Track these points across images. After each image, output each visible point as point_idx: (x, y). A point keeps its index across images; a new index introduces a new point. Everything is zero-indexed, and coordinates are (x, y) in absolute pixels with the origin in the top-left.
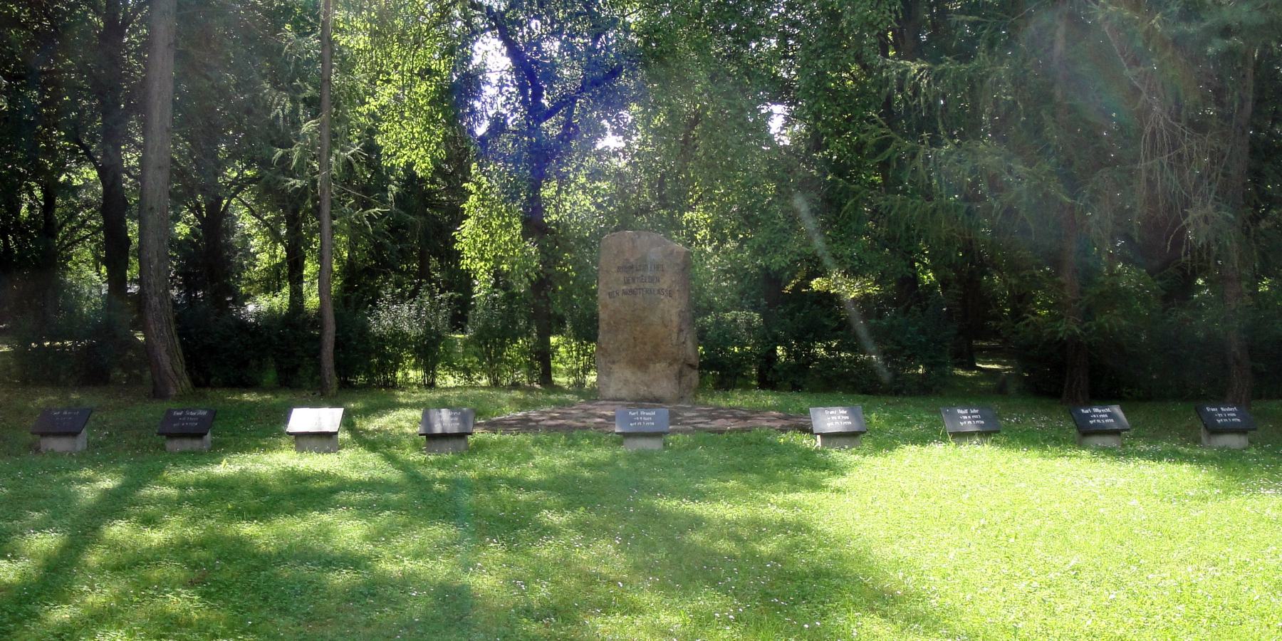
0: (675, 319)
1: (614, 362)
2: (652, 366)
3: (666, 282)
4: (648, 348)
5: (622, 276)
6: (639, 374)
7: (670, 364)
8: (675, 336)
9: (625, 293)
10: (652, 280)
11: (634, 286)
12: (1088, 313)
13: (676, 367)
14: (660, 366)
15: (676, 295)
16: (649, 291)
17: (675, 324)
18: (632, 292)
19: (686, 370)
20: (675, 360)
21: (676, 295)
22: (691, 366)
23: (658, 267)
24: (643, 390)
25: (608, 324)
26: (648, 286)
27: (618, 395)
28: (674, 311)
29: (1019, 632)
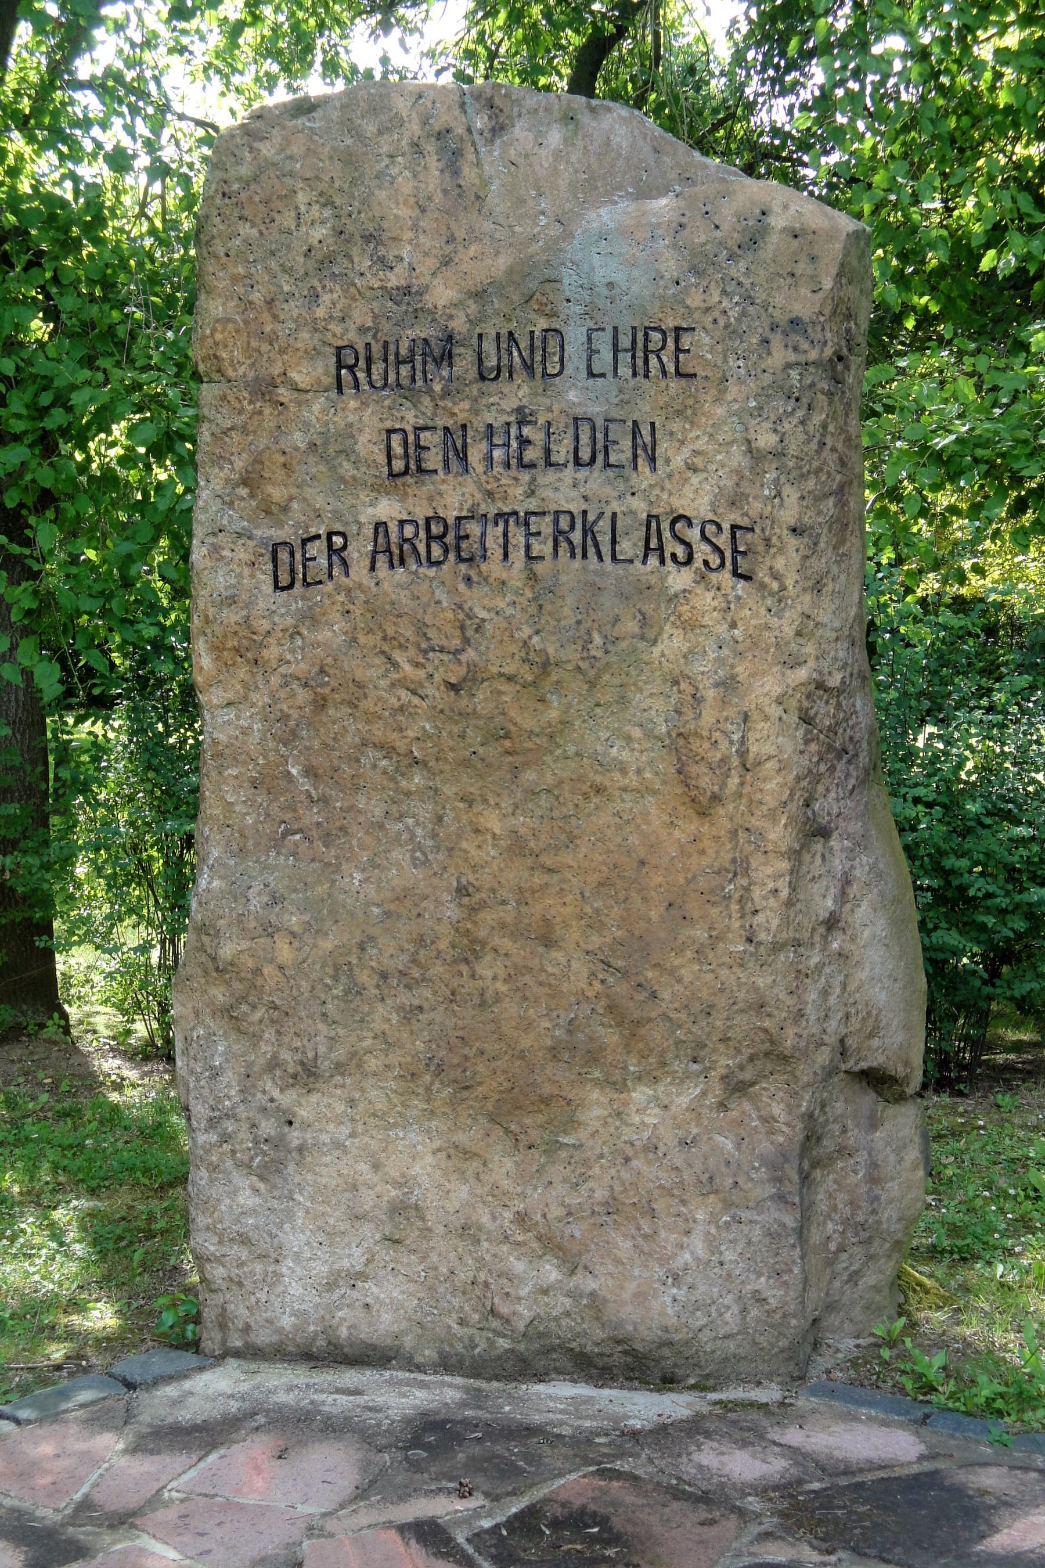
0: (775, 743)
1: (307, 1075)
2: (595, 1105)
3: (704, 463)
4: (572, 968)
5: (367, 421)
6: (503, 1166)
7: (737, 1088)
8: (769, 873)
9: (391, 549)
10: (594, 455)
11: (454, 496)
12: (979, 351)
13: (777, 1108)
14: (657, 1109)
15: (786, 561)
16: (581, 535)
17: (773, 786)
18: (446, 541)
19: (847, 1105)
20: (774, 1056)
21: (786, 561)
22: (878, 1081)
23: (650, 347)
24: (534, 1289)
25: (268, 782)
26: (564, 491)
27: (349, 1323)
28: (768, 686)
29: (835, 681)
